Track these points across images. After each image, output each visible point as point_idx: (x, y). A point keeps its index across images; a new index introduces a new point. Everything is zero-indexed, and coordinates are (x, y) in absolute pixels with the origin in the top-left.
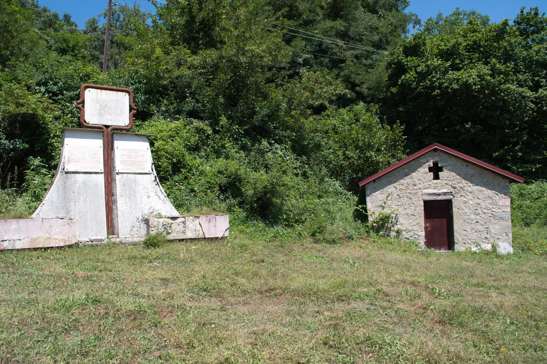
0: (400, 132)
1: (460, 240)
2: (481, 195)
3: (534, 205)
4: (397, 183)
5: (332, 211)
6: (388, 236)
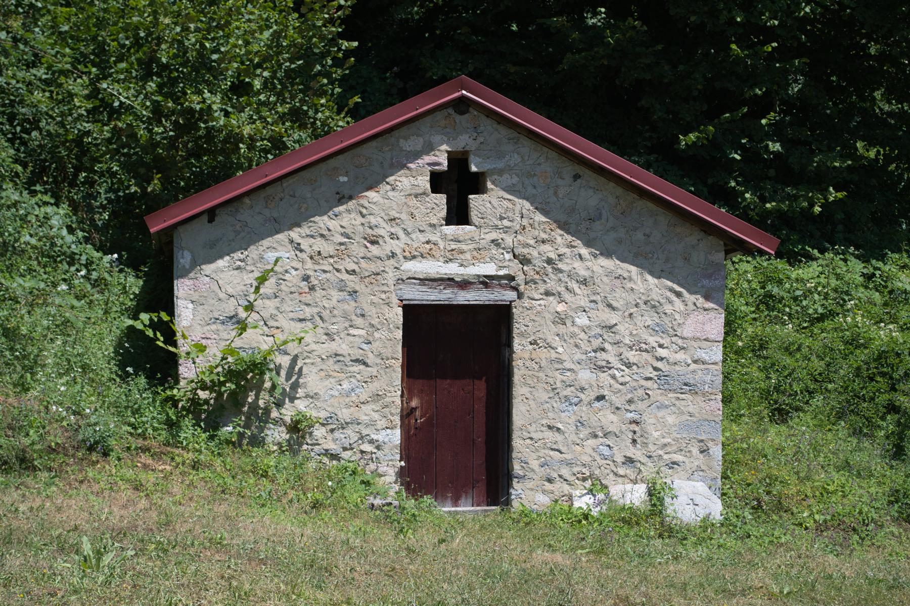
0: (331, 21)
1: (534, 464)
2: (619, 293)
3: (808, 342)
4: (305, 230)
5: (24, 330)
6: (257, 441)
